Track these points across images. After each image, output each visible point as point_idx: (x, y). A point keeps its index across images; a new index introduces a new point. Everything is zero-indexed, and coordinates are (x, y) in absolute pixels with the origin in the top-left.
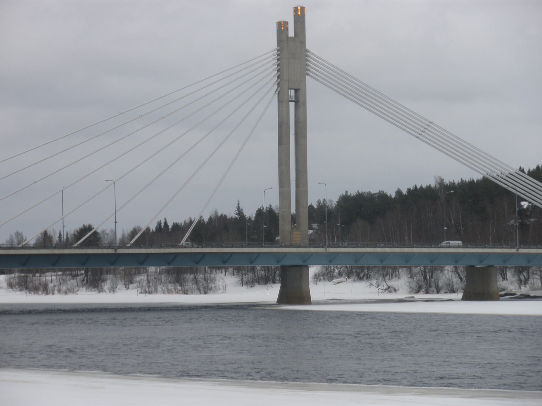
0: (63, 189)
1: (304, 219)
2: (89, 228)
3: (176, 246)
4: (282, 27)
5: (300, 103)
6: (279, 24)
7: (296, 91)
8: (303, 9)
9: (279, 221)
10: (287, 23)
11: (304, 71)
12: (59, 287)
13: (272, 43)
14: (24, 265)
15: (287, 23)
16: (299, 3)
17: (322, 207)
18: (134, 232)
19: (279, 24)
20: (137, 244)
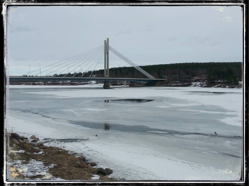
0: (44, 141)
1: (108, 70)
2: (56, 74)
3: (89, 77)
4: (105, 41)
5: (108, 54)
6: (105, 41)
7: (107, 52)
8: (108, 38)
9: (190, 63)
10: (106, 41)
11: (108, 49)
12: (29, 177)
13: (104, 44)
14: (42, 80)
15: (106, 41)
16: (108, 38)
17: (110, 69)
18: (75, 73)
19: (105, 41)
20: (75, 77)
